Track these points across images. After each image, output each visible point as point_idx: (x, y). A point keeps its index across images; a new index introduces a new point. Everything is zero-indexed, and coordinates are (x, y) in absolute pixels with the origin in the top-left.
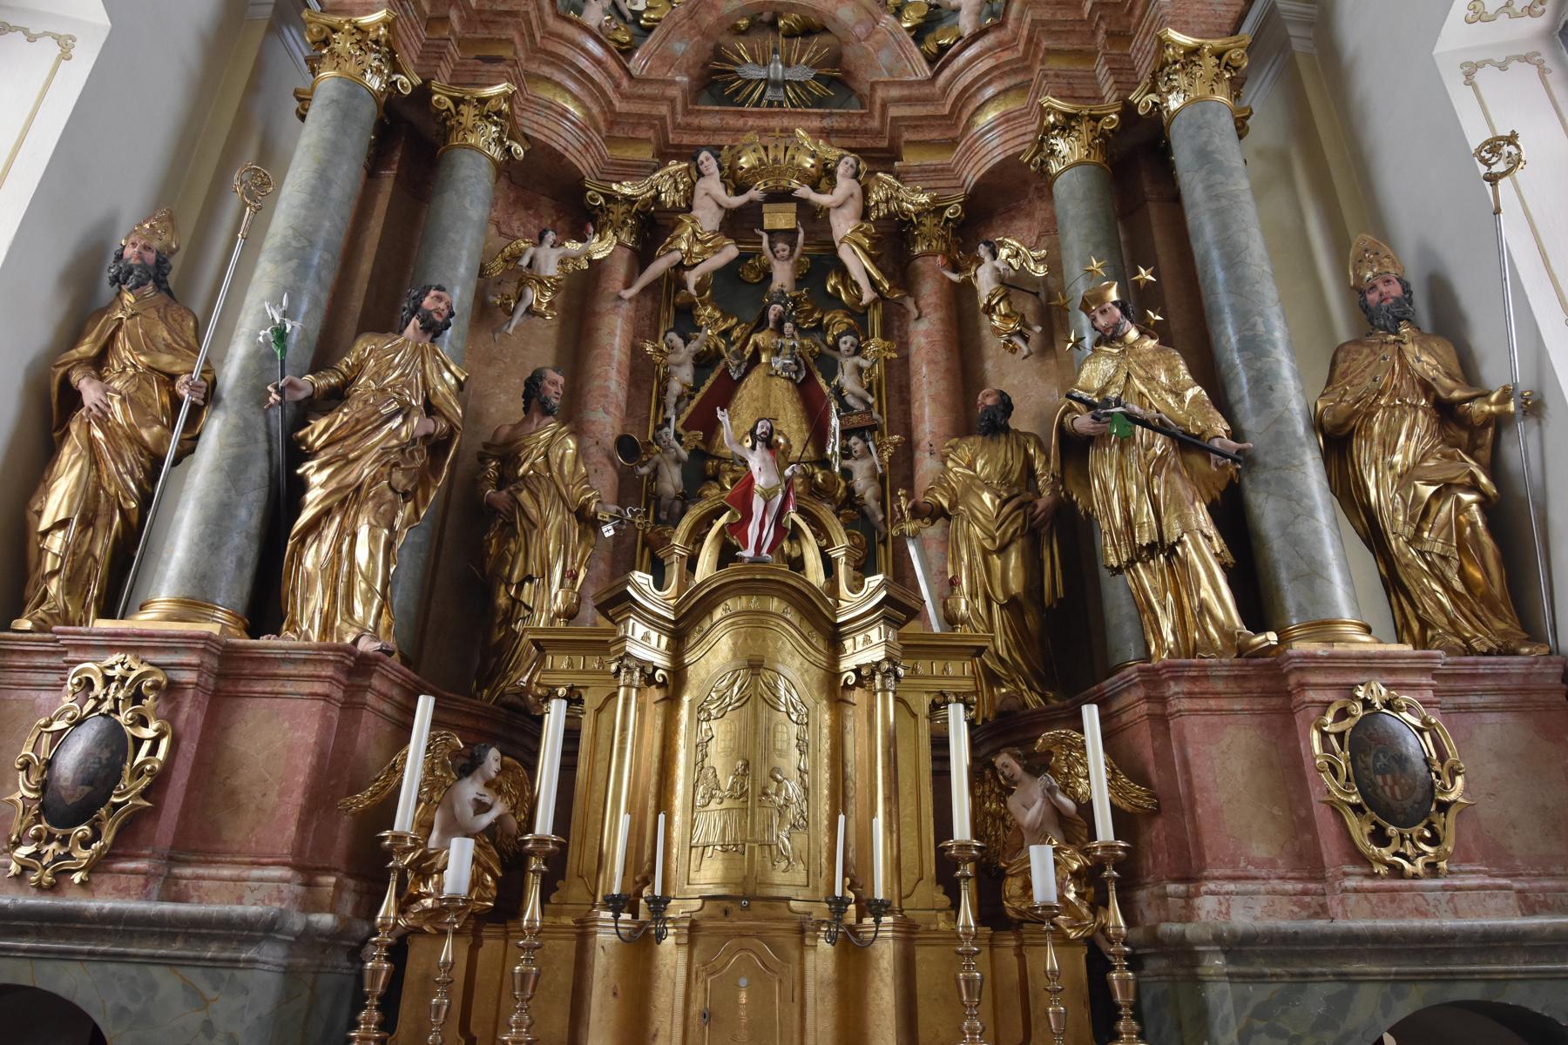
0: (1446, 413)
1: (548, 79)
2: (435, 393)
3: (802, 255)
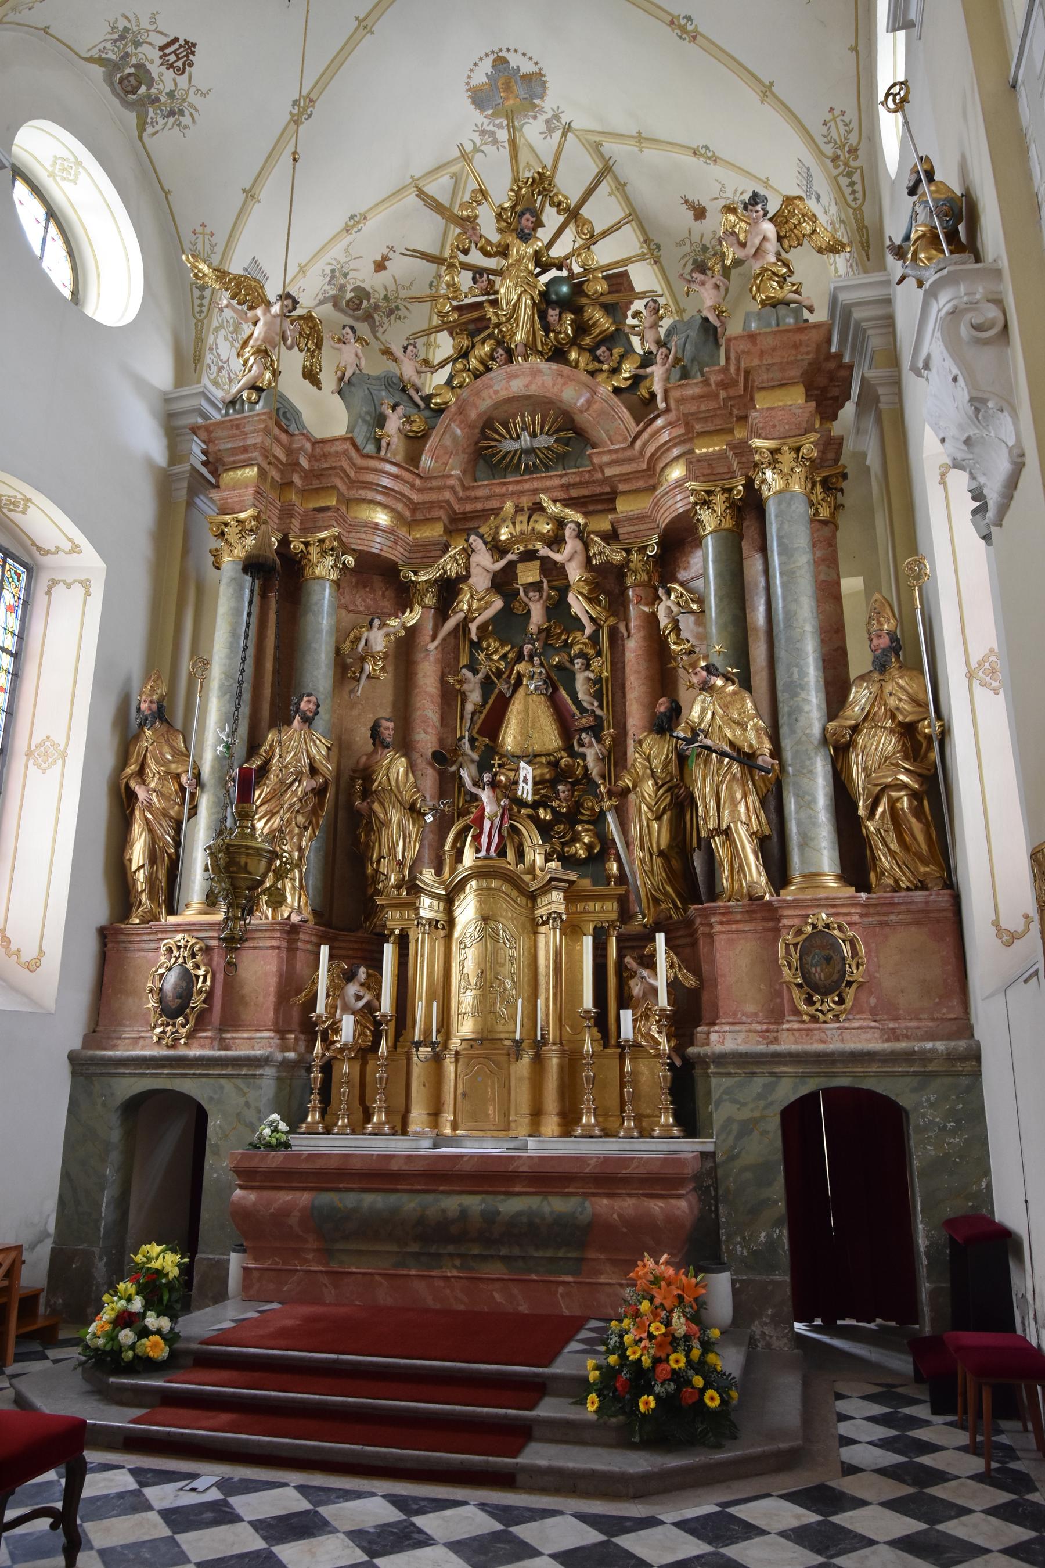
0: (908, 731)
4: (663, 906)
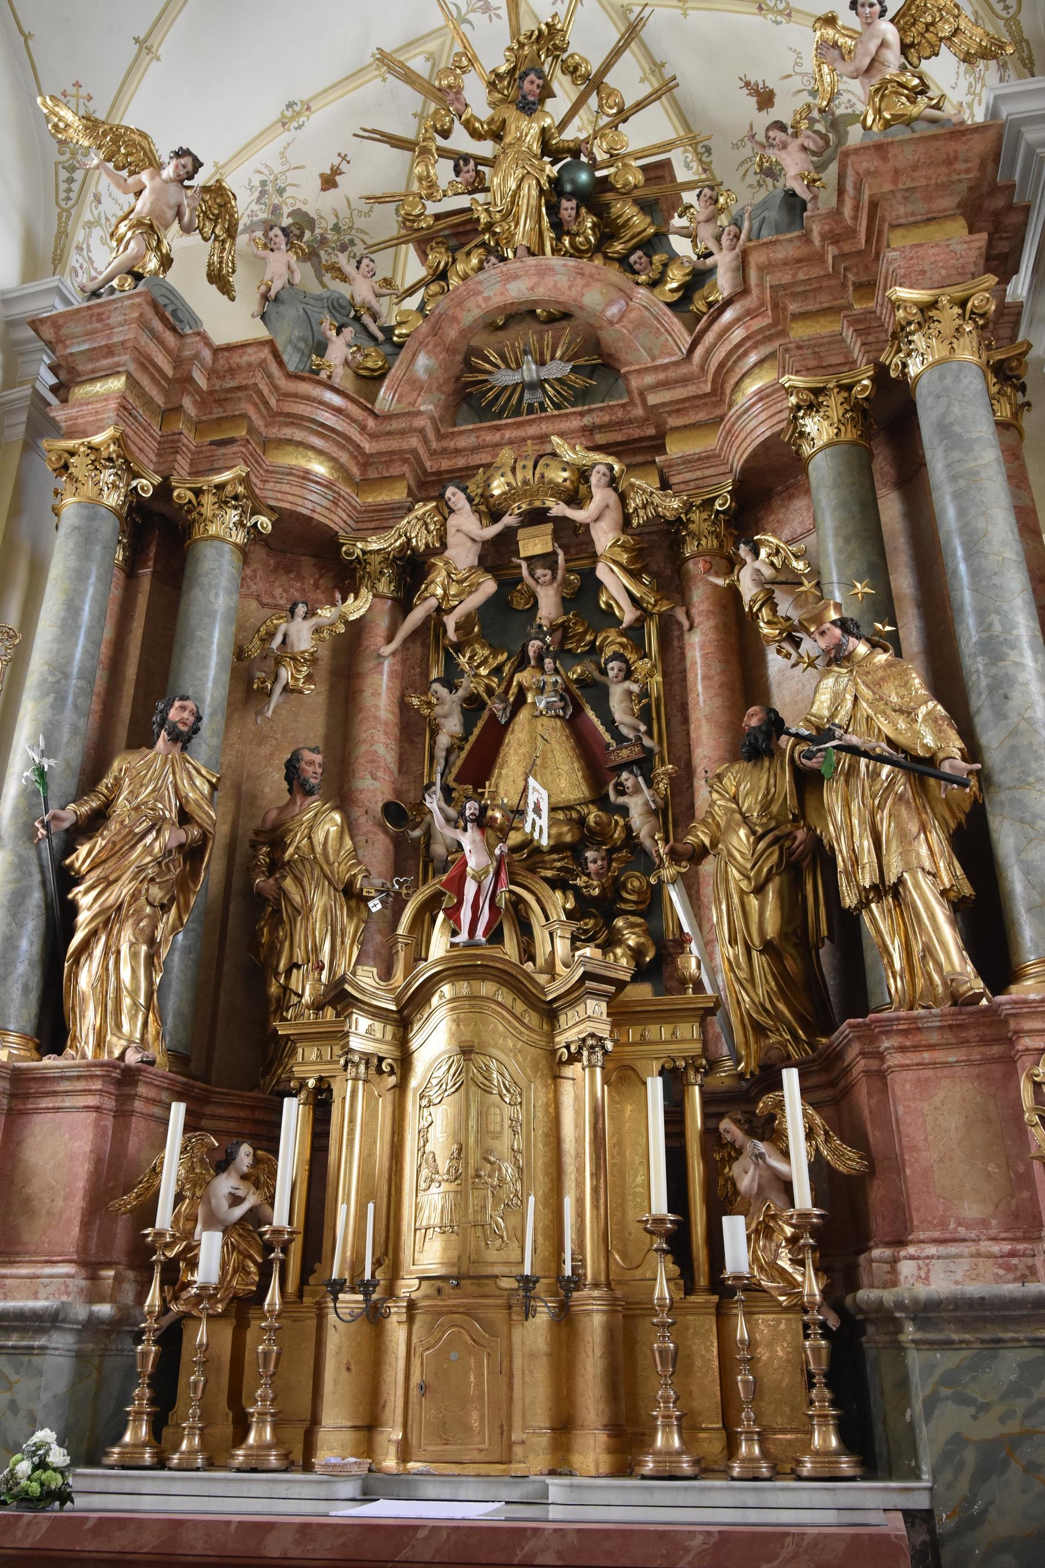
1: (290, 442)
2: (187, 800)
3: (569, 571)
4: (773, 1039)
